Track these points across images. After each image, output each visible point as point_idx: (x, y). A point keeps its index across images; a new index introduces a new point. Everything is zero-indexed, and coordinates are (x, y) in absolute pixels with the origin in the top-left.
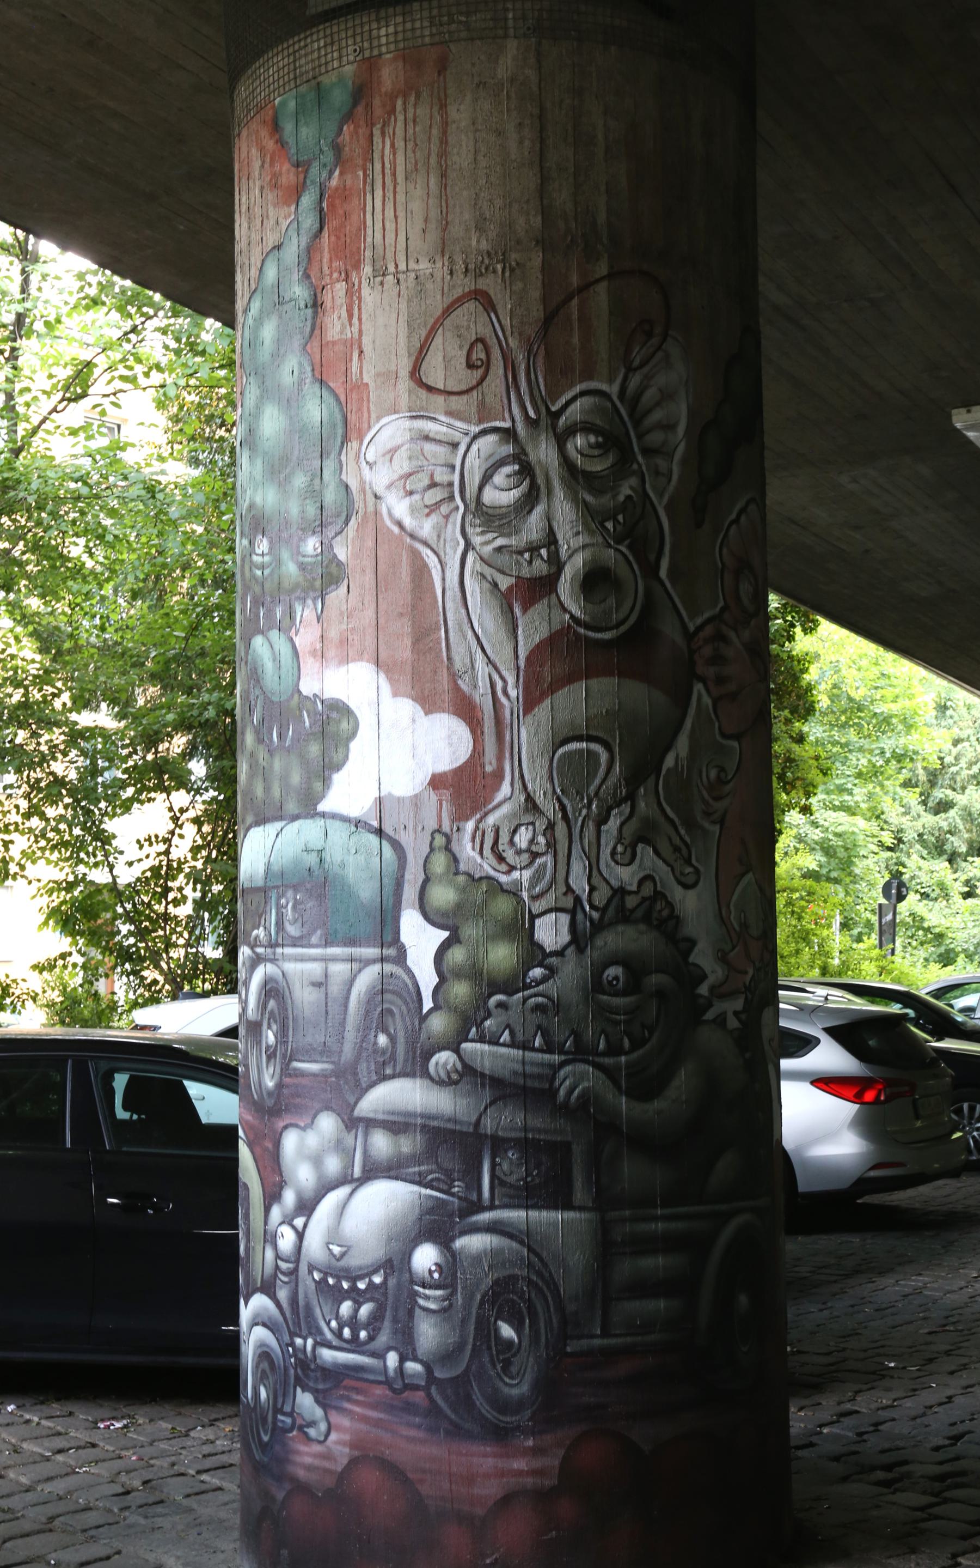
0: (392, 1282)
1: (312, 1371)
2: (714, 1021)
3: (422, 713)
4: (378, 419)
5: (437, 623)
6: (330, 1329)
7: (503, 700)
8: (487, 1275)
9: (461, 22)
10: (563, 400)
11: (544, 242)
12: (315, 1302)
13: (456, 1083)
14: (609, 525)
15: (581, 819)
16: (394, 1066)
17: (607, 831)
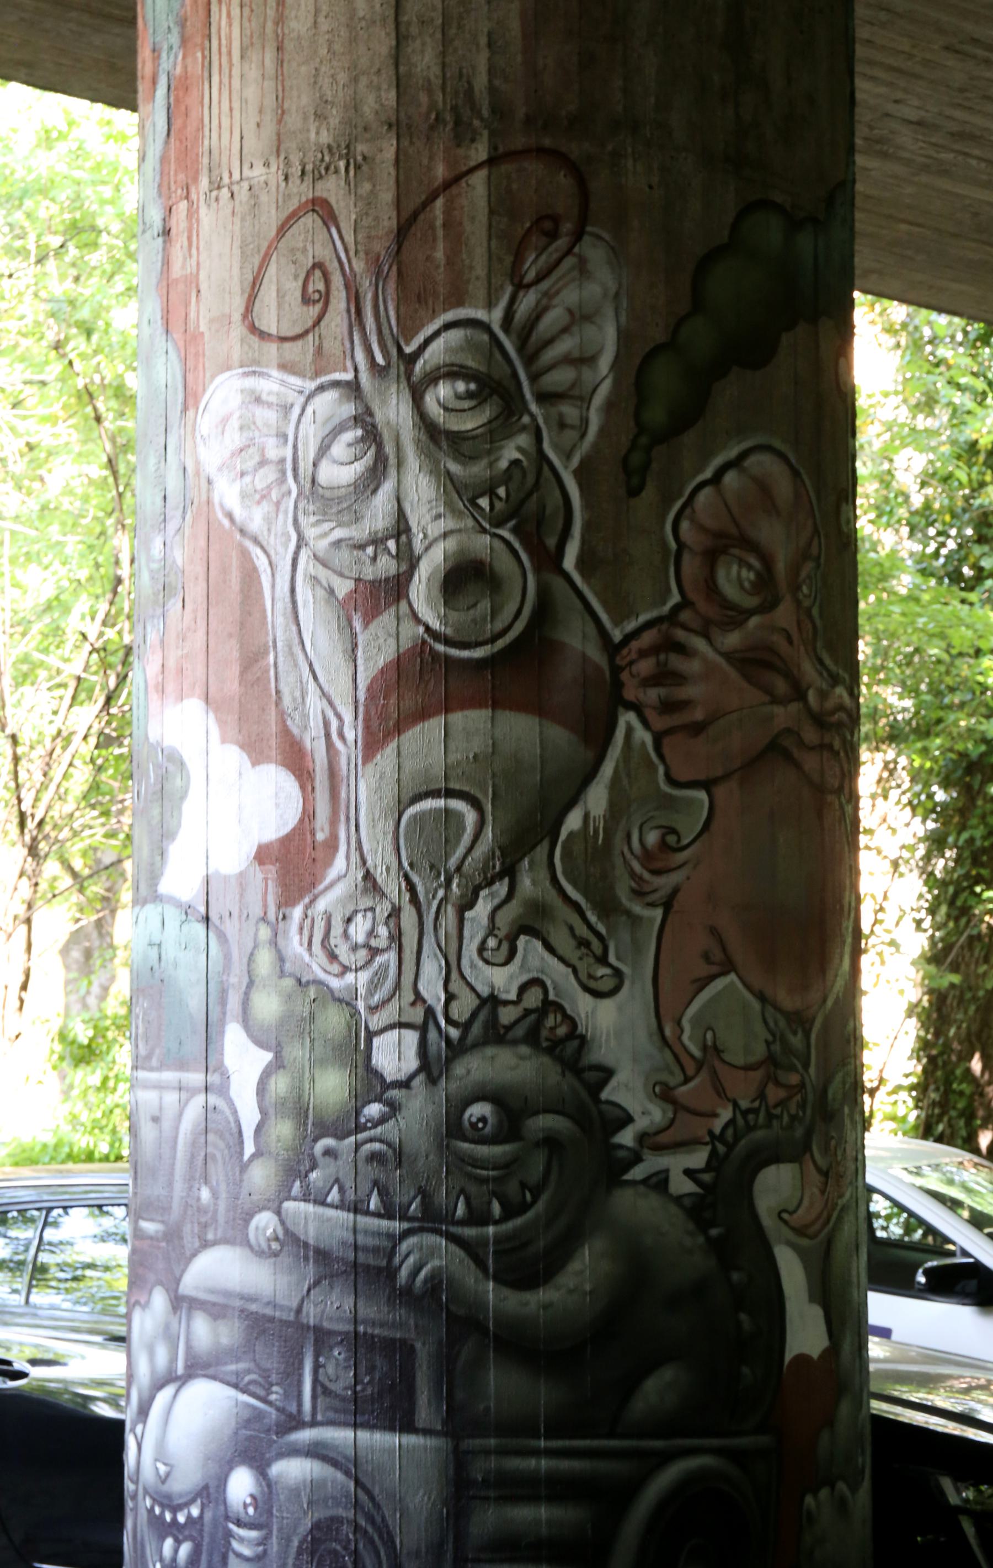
0: (208, 1516)
2: (645, 1181)
3: (249, 764)
4: (213, 377)
8: (305, 1513)
10: (420, 338)
11: (399, 126)
12: (146, 1538)
13: (276, 1255)
14: (484, 502)
16: (216, 1229)
17: (473, 920)
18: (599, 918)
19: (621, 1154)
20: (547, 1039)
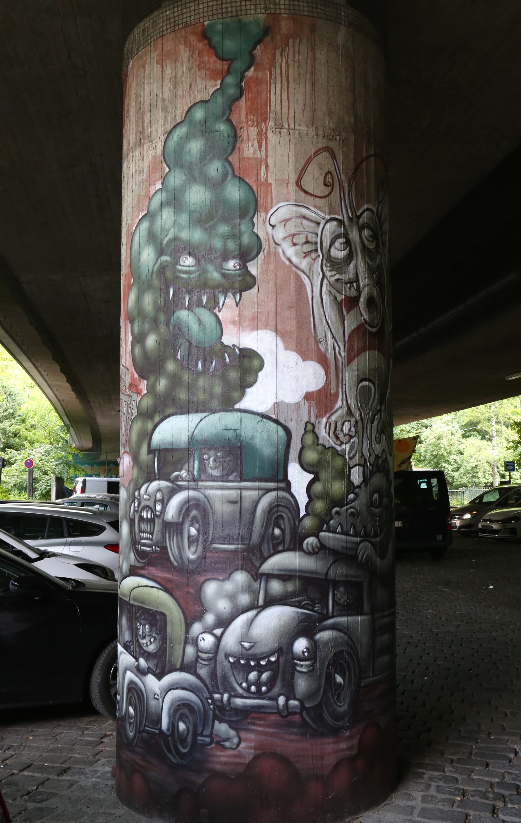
0: (282, 660)
1: (228, 711)
3: (301, 360)
4: (278, 203)
6: (242, 688)
8: (331, 652)
9: (321, 9)
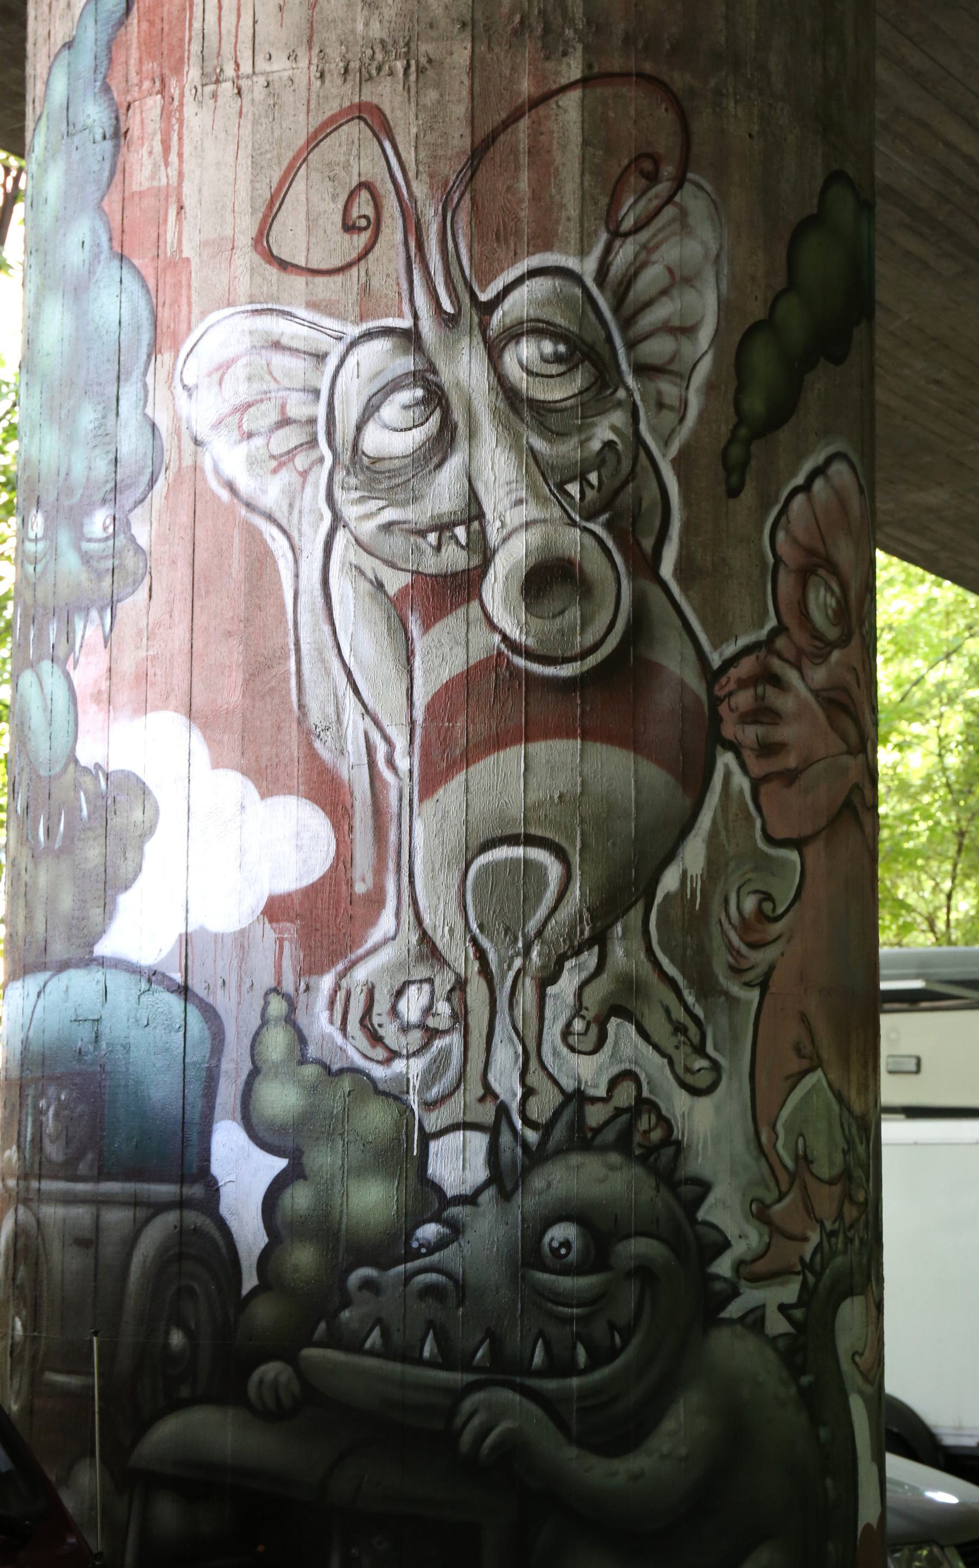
2: (741, 1319)
3: (255, 794)
4: (204, 314)
5: (284, 647)
7: (387, 774)
14: (574, 489)
15: (511, 974)
17: (556, 997)
18: (698, 999)
19: (718, 1286)
20: (640, 1146)
